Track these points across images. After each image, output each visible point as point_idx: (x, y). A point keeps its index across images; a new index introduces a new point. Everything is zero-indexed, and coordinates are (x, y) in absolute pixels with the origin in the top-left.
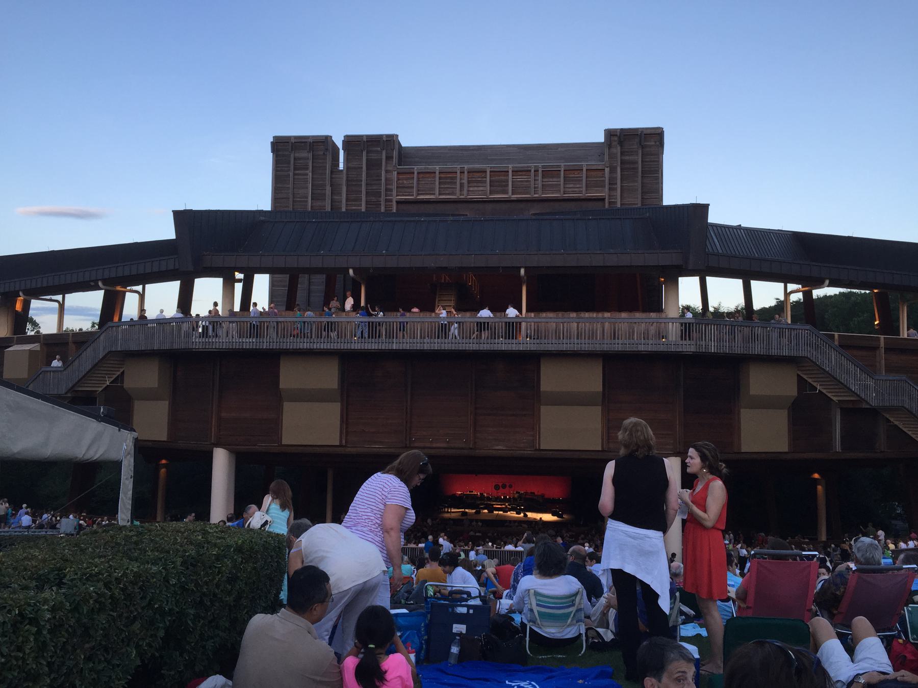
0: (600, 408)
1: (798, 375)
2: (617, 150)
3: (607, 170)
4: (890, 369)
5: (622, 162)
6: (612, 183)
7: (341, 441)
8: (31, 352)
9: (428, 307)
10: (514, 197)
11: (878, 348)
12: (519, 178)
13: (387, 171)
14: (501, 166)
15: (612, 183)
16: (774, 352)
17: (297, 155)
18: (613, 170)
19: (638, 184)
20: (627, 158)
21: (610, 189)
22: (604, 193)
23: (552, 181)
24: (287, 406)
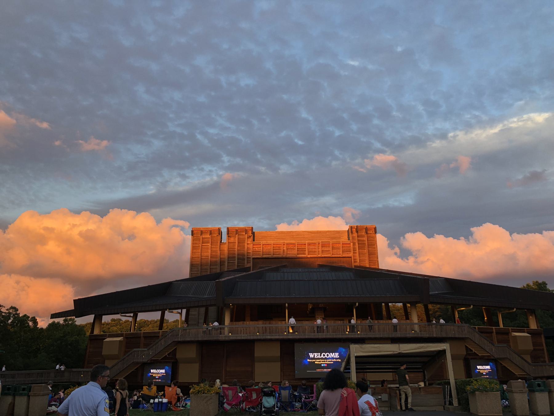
0: (279, 363)
1: (466, 347)
2: (355, 235)
3: (352, 244)
4: (499, 342)
5: (358, 240)
6: (354, 250)
7: (421, 372)
8: (120, 341)
9: (314, 318)
10: (309, 256)
11: (493, 332)
12: (311, 247)
13: (248, 244)
14: (303, 242)
15: (354, 250)
16: (457, 336)
17: (204, 236)
18: (354, 244)
19: (366, 251)
20: (359, 238)
21: (354, 253)
22: (351, 255)
23: (325, 249)
24: (257, 365)
